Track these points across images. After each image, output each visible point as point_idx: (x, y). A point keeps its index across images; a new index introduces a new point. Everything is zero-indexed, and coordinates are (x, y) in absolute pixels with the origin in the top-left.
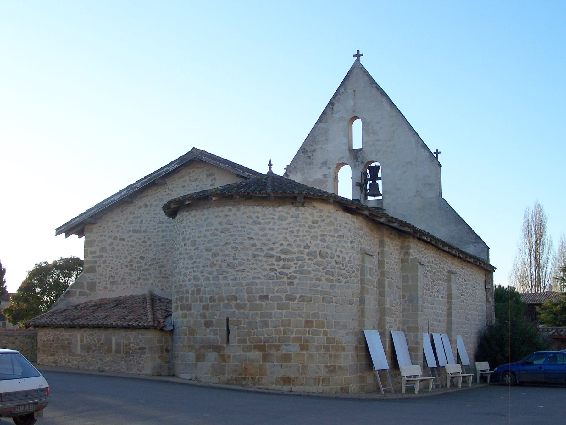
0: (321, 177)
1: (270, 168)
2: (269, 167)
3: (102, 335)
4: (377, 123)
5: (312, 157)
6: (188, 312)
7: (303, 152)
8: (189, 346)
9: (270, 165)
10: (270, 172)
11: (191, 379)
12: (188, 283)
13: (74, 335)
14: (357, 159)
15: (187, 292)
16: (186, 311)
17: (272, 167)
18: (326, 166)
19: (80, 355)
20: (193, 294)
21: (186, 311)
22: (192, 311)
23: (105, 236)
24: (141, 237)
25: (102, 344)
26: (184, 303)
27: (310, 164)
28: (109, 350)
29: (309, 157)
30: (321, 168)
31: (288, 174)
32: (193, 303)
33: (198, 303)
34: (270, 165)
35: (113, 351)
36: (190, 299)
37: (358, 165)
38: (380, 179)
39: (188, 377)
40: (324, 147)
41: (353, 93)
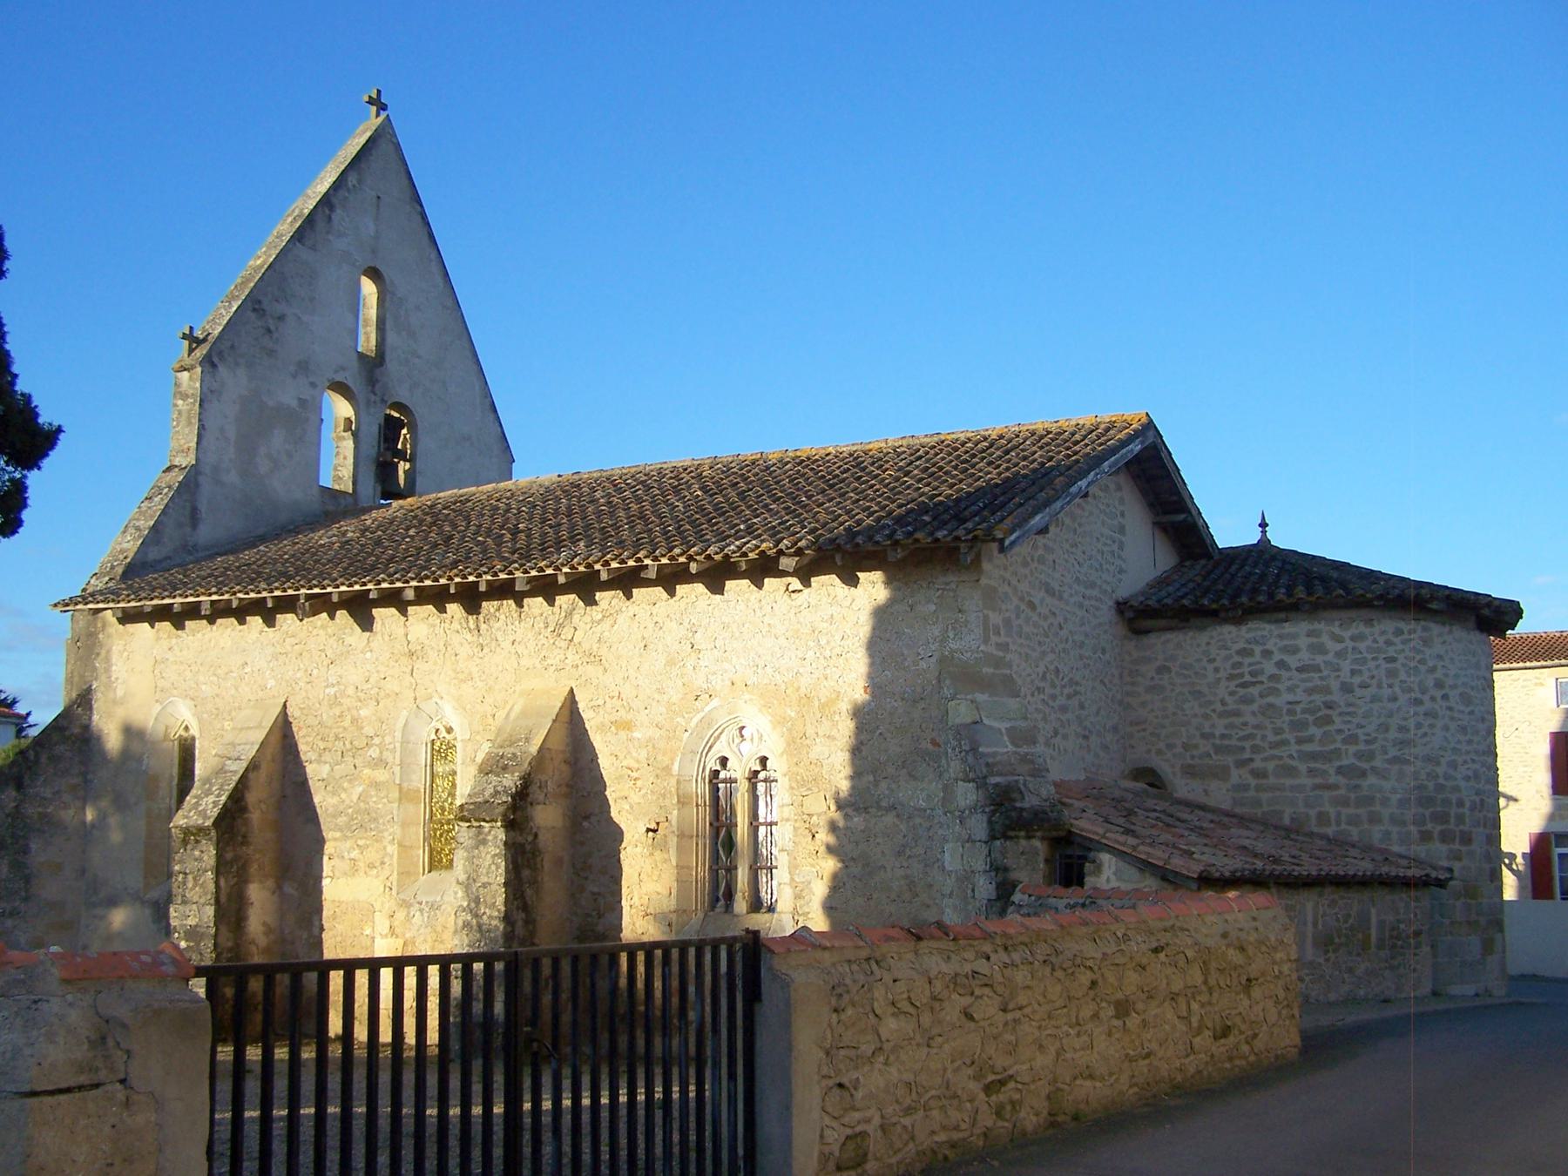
0: (294, 403)
1: (1264, 532)
2: (1261, 529)
3: (1354, 901)
4: (418, 308)
5: (275, 335)
6: (1463, 848)
7: (254, 310)
8: (1469, 923)
9: (1263, 525)
10: (1264, 542)
11: (1477, 995)
12: (1462, 784)
13: (1298, 907)
14: (373, 386)
15: (1460, 804)
16: (1457, 846)
17: (1267, 529)
18: (307, 377)
19: (1311, 963)
20: (1472, 809)
21: (1457, 846)
22: (1473, 847)
23: (1015, 589)
24: (1057, 612)
25: (1351, 928)
26: (1452, 826)
27: (271, 353)
28: (1365, 945)
29: (269, 331)
30: (294, 376)
31: (215, 360)
32: (1474, 830)
33: (1481, 829)
34: (1263, 525)
35: (1373, 945)
36: (1467, 820)
37: (375, 402)
38: (402, 455)
39: (1469, 990)
40: (305, 318)
41: (375, 200)
